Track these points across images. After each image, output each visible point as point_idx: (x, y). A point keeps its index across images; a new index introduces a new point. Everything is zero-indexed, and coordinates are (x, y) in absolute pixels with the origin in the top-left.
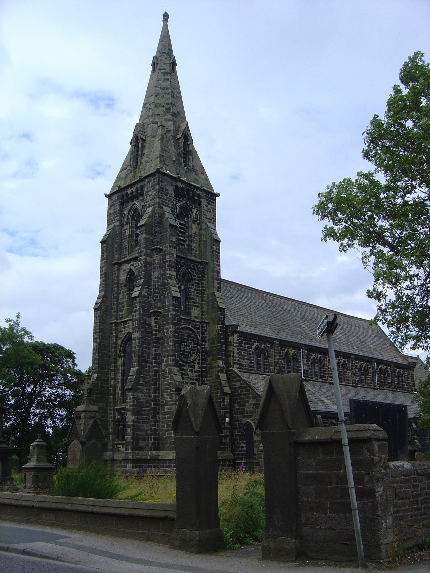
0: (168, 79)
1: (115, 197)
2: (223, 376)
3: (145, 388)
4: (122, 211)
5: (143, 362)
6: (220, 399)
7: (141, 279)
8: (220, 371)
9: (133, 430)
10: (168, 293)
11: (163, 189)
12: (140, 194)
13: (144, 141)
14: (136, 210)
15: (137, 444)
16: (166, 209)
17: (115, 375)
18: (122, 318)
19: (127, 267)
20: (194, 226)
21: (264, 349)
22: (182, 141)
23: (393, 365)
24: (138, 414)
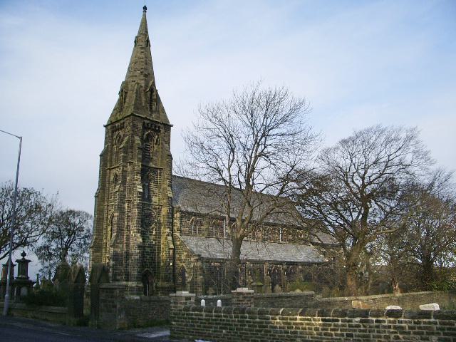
1: (109, 127)
2: (170, 238)
3: (121, 246)
4: (112, 136)
5: (120, 231)
8: (168, 235)
12: (122, 127)
13: (126, 93)
16: (137, 138)
17: (107, 236)
19: (114, 171)
20: (156, 146)
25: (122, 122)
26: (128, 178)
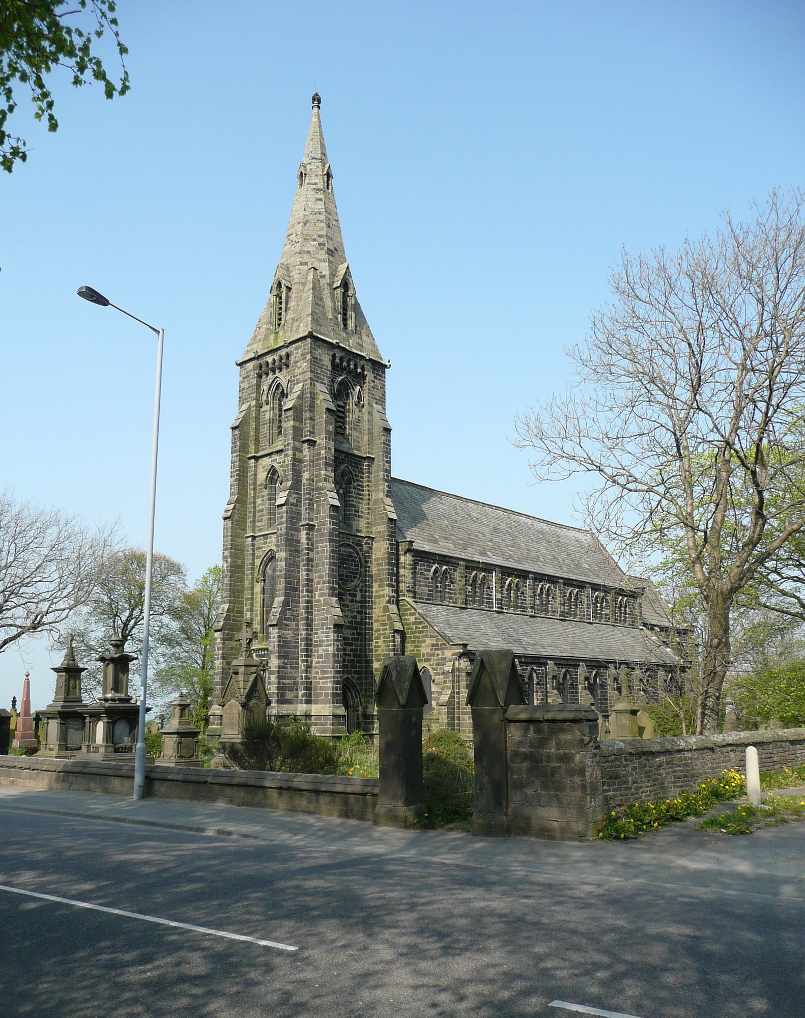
0: (321, 200)
1: (250, 365)
3: (293, 624)
4: (258, 386)
5: (291, 590)
6: (389, 637)
7: (288, 480)
9: (279, 677)
10: (324, 501)
11: (317, 358)
12: (284, 363)
15: (283, 695)
16: (320, 387)
17: (252, 605)
18: (261, 530)
19: (266, 462)
21: (445, 572)
22: (339, 292)
24: (284, 658)
25: (283, 352)
26: (306, 475)
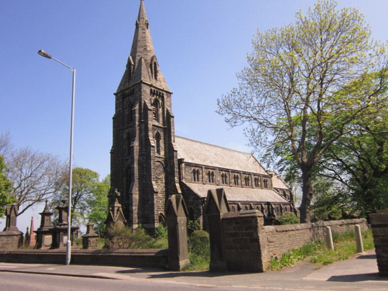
1: (119, 95)
14: (130, 102)
19: (127, 130)
23: (261, 176)
